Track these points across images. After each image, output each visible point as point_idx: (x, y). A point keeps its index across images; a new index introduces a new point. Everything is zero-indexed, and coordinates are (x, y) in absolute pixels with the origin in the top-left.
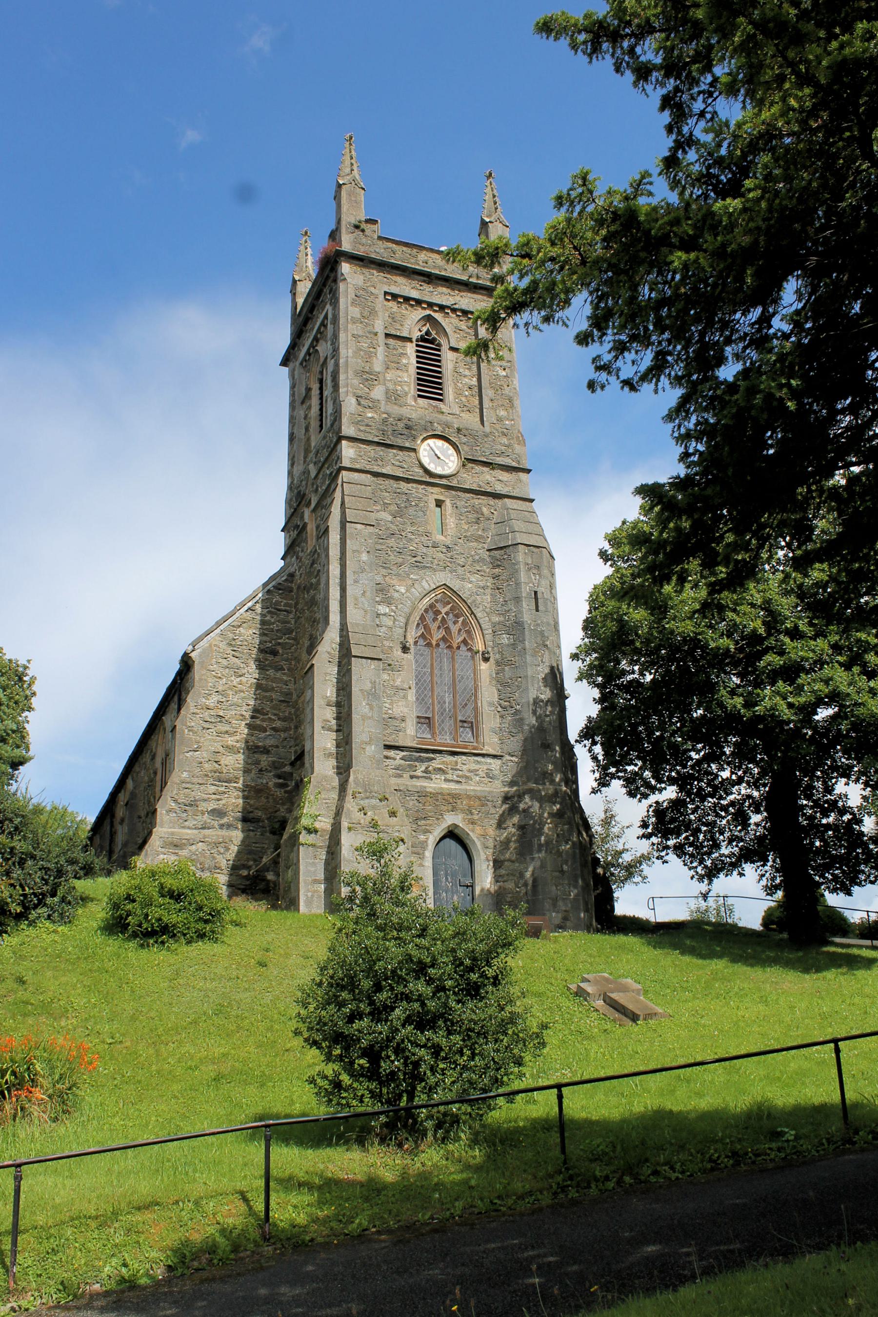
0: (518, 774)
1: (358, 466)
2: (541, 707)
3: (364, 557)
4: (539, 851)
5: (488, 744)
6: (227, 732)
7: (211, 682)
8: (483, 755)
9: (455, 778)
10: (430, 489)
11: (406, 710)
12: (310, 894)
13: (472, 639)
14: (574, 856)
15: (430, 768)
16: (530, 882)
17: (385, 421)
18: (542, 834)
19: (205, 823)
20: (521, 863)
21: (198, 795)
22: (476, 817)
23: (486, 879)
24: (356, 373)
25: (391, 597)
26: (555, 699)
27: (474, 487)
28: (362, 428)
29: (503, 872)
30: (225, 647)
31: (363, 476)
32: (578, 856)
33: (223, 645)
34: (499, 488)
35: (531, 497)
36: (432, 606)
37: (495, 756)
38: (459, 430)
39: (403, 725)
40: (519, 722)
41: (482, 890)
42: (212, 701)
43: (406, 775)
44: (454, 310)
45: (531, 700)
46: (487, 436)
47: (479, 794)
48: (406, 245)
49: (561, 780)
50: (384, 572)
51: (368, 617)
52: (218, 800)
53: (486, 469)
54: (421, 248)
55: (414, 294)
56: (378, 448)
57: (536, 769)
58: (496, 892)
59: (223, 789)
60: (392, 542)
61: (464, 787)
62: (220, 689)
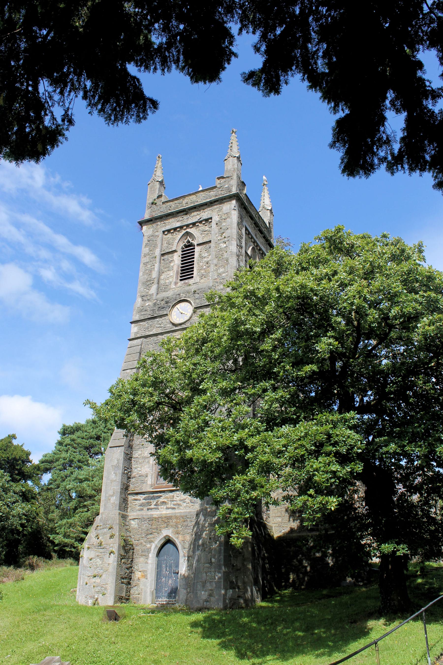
1: (138, 336)
4: (198, 549)
11: (148, 470)
14: (220, 552)
17: (155, 304)
18: (200, 539)
23: (183, 569)
28: (143, 313)
32: (223, 551)
38: (195, 292)
43: (145, 509)
44: (201, 222)
48: (177, 199)
54: (184, 197)
55: (178, 224)
56: (149, 321)
61: (177, 511)
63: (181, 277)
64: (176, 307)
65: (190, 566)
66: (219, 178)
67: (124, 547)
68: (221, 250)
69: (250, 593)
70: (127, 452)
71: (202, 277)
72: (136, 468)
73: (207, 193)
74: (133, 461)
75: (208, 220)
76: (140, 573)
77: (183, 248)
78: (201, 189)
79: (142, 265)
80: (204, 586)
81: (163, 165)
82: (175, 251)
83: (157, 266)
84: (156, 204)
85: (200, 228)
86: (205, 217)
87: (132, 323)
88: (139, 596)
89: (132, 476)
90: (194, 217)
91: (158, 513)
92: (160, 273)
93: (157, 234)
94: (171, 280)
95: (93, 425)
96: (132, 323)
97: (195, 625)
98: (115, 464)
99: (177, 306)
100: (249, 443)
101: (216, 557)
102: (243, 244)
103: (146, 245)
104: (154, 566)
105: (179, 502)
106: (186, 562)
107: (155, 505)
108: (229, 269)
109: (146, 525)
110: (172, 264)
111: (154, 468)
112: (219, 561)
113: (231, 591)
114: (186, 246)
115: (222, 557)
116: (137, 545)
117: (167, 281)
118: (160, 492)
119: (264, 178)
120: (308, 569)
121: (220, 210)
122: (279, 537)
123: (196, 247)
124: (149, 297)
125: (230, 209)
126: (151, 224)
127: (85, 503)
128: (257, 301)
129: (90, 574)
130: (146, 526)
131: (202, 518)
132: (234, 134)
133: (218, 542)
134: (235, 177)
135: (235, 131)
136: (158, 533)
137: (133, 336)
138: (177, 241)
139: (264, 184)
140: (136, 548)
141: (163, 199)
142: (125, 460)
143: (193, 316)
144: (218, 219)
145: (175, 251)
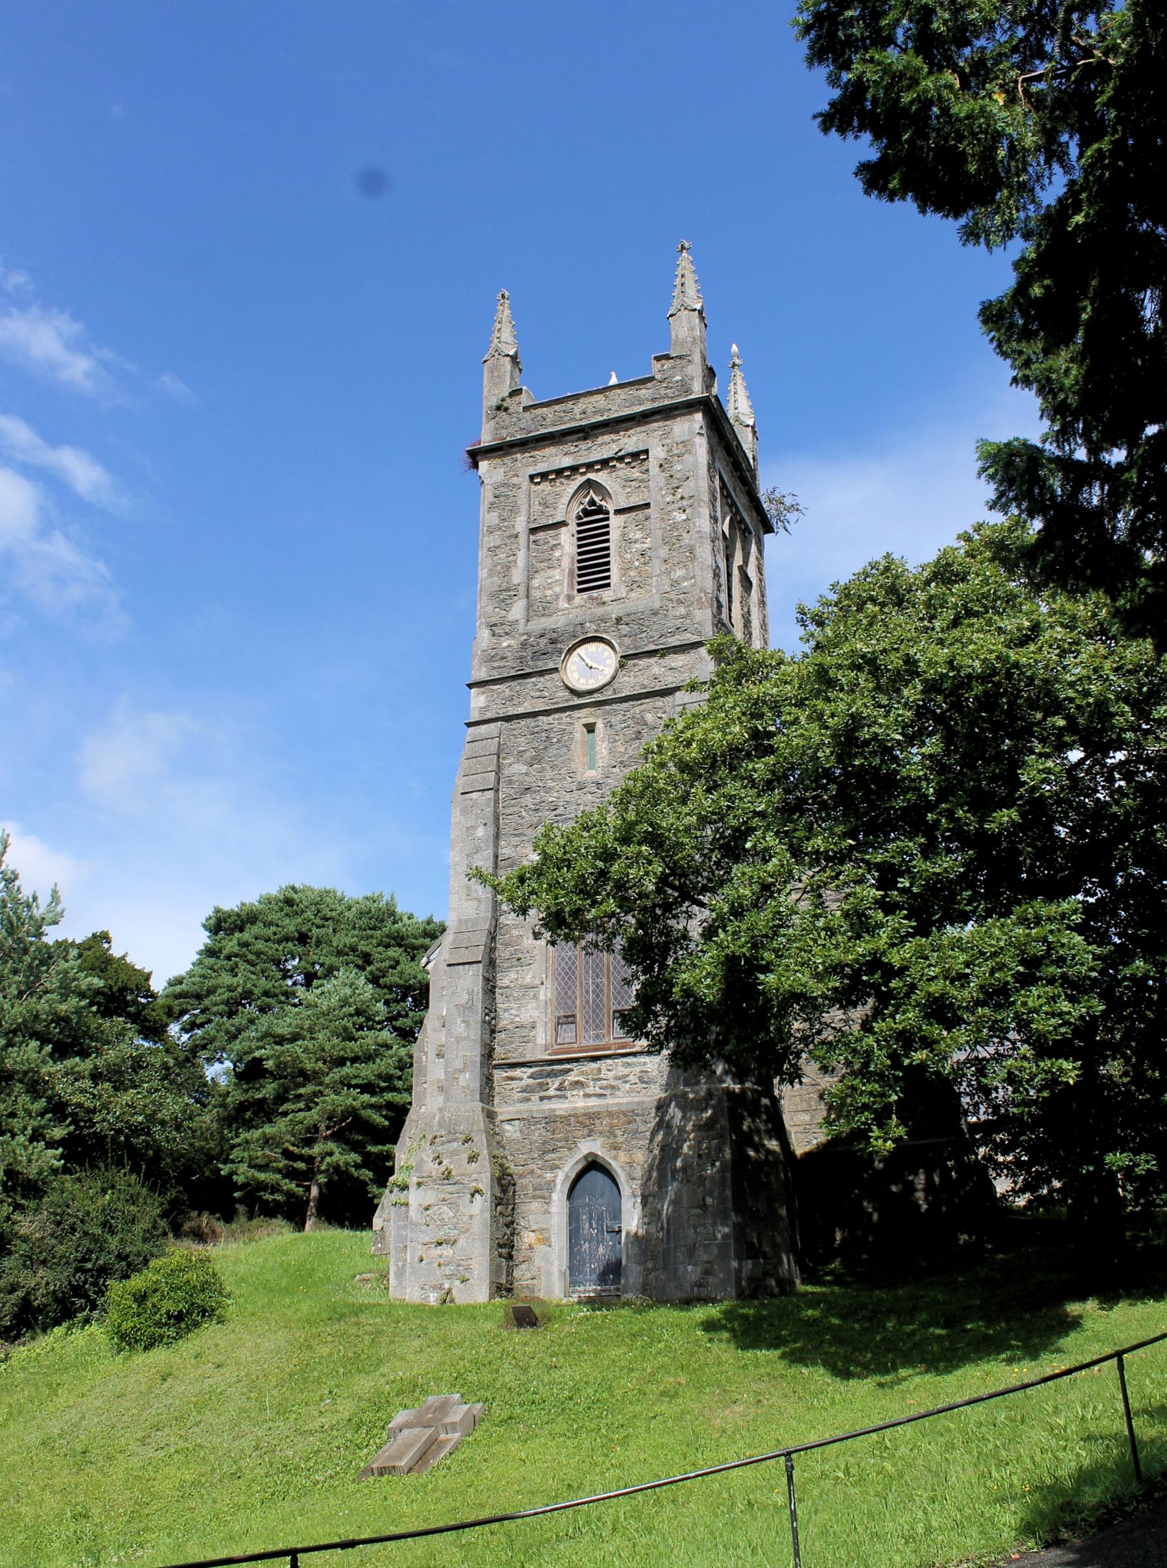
1: (489, 715)
4: (674, 1179)
11: (536, 1013)
12: (400, 1264)
14: (723, 1184)
15: (567, 1083)
17: (524, 645)
22: (621, 1139)
23: (632, 1220)
28: (496, 664)
32: (729, 1182)
34: (670, 680)
38: (619, 620)
39: (533, 1033)
41: (628, 1234)
44: (620, 459)
47: (624, 1108)
49: (726, 1072)
53: (652, 660)
54: (576, 397)
55: (567, 462)
60: (528, 800)
61: (610, 1101)
63: (579, 583)
64: (575, 653)
65: (651, 1213)
66: (658, 359)
67: (499, 1179)
68: (675, 526)
69: (786, 1266)
70: (487, 975)
71: (632, 585)
72: (506, 1010)
73: (631, 392)
74: (497, 996)
75: (639, 456)
76: (532, 1234)
77: (579, 518)
78: (614, 381)
79: (482, 553)
81: (514, 316)
82: (563, 524)
83: (521, 555)
84: (506, 409)
85: (620, 473)
86: (632, 449)
87: (470, 686)
88: (534, 1282)
89: (499, 1028)
90: (605, 446)
91: (566, 1106)
92: (531, 572)
93: (515, 480)
94: (557, 589)
95: (287, 909)
96: (470, 686)
97: (710, 1326)
98: (463, 1002)
99: (578, 650)
100: (895, 958)
101: (716, 1194)
102: (719, 514)
103: (491, 508)
104: (565, 1219)
106: (639, 1207)
107: (557, 1089)
108: (697, 572)
109: (538, 1134)
110: (557, 554)
111: (549, 1010)
112: (723, 1201)
113: (750, 1262)
114: (586, 513)
115: (728, 1193)
116: (521, 1176)
117: (549, 592)
118: (569, 1061)
119: (734, 348)
120: (875, 1217)
121: (666, 435)
122: (807, 1155)
123: (611, 515)
124: (507, 629)
125: (691, 432)
126: (500, 457)
127: (302, 1091)
128: (886, 678)
129: (427, 1239)
130: (540, 1135)
131: (675, 1113)
132: (684, 254)
133: (718, 1164)
134: (697, 358)
135: (686, 245)
136: (570, 1149)
137: (475, 717)
138: (565, 500)
139: (734, 365)
140: (521, 1182)
141: (525, 399)
142: (485, 992)
143: (620, 674)
144: (662, 455)
145: (563, 524)
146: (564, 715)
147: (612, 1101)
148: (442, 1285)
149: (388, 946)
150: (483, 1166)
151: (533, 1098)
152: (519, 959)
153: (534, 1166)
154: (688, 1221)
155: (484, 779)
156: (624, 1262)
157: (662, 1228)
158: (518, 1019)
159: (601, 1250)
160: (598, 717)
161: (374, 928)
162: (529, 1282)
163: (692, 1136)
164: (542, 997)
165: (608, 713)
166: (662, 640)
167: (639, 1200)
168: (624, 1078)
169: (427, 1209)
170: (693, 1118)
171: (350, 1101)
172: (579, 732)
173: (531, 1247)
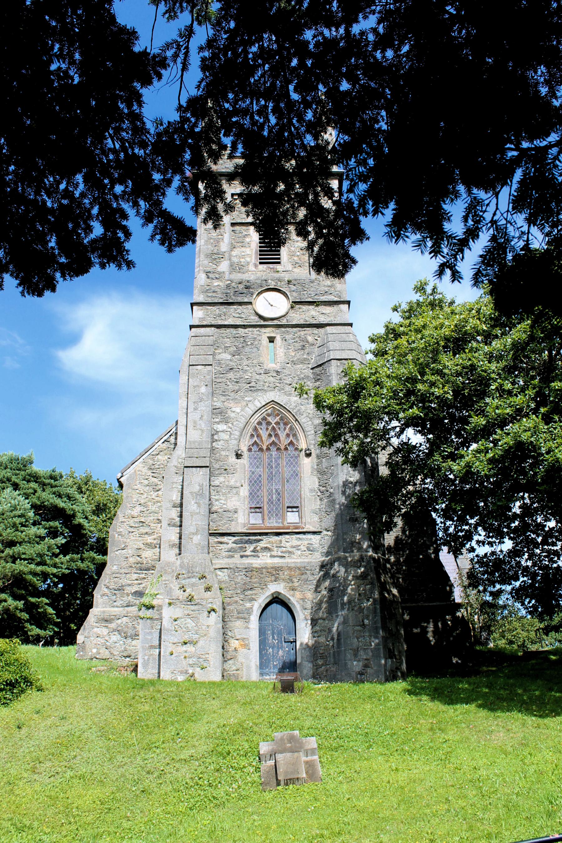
0: (332, 546)
1: (205, 323)
2: (350, 488)
3: (203, 389)
4: (343, 609)
5: (310, 523)
6: (147, 533)
7: (135, 497)
8: (304, 533)
9: (280, 554)
10: (263, 330)
11: (238, 503)
12: (146, 658)
13: (298, 440)
15: (258, 548)
16: (336, 637)
17: (228, 286)
18: (344, 595)
19: (129, 602)
20: (329, 620)
21: (124, 581)
22: (296, 584)
23: (305, 635)
24: (207, 256)
25: (229, 417)
26: (363, 479)
27: (302, 322)
28: (210, 295)
29: (317, 628)
30: (146, 471)
31: (208, 329)
32: (379, 611)
33: (145, 470)
34: (323, 320)
35: (350, 322)
36: (264, 419)
37: (314, 533)
38: (289, 282)
39: (236, 515)
40: (333, 502)
41: (301, 644)
42: (135, 512)
43: (237, 556)
45: (341, 483)
46: (312, 282)
47: (299, 565)
49: (369, 546)
50: (223, 398)
51: (204, 435)
52: (140, 584)
53: (311, 307)
56: (222, 307)
57: (344, 540)
58: (313, 645)
59: (143, 576)
60: (231, 375)
61: (287, 560)
62: (142, 502)
72: (216, 500)
76: (237, 641)
80: (356, 655)
94: (248, 259)
105: (290, 550)
106: (309, 627)
107: (253, 551)
109: (240, 578)
110: (248, 240)
111: (246, 503)
112: (375, 623)
115: (378, 618)
117: (242, 260)
129: (176, 640)
131: (338, 569)
137: (197, 323)
146: (255, 329)
147: (289, 561)
148: (187, 671)
149: (29, 481)
150: (216, 594)
151: (236, 556)
152: (226, 470)
153: (238, 599)
154: (353, 634)
155: (206, 359)
156: (299, 661)
157: (332, 639)
158: (225, 506)
159: (281, 653)
160: (277, 333)
161: (19, 470)
162: (235, 672)
163: (353, 583)
164: (241, 494)
165: (284, 332)
166: (316, 297)
167: (309, 622)
168: (297, 547)
169: (175, 620)
170: (352, 572)
171: (22, 568)
172: (265, 341)
173: (236, 650)
